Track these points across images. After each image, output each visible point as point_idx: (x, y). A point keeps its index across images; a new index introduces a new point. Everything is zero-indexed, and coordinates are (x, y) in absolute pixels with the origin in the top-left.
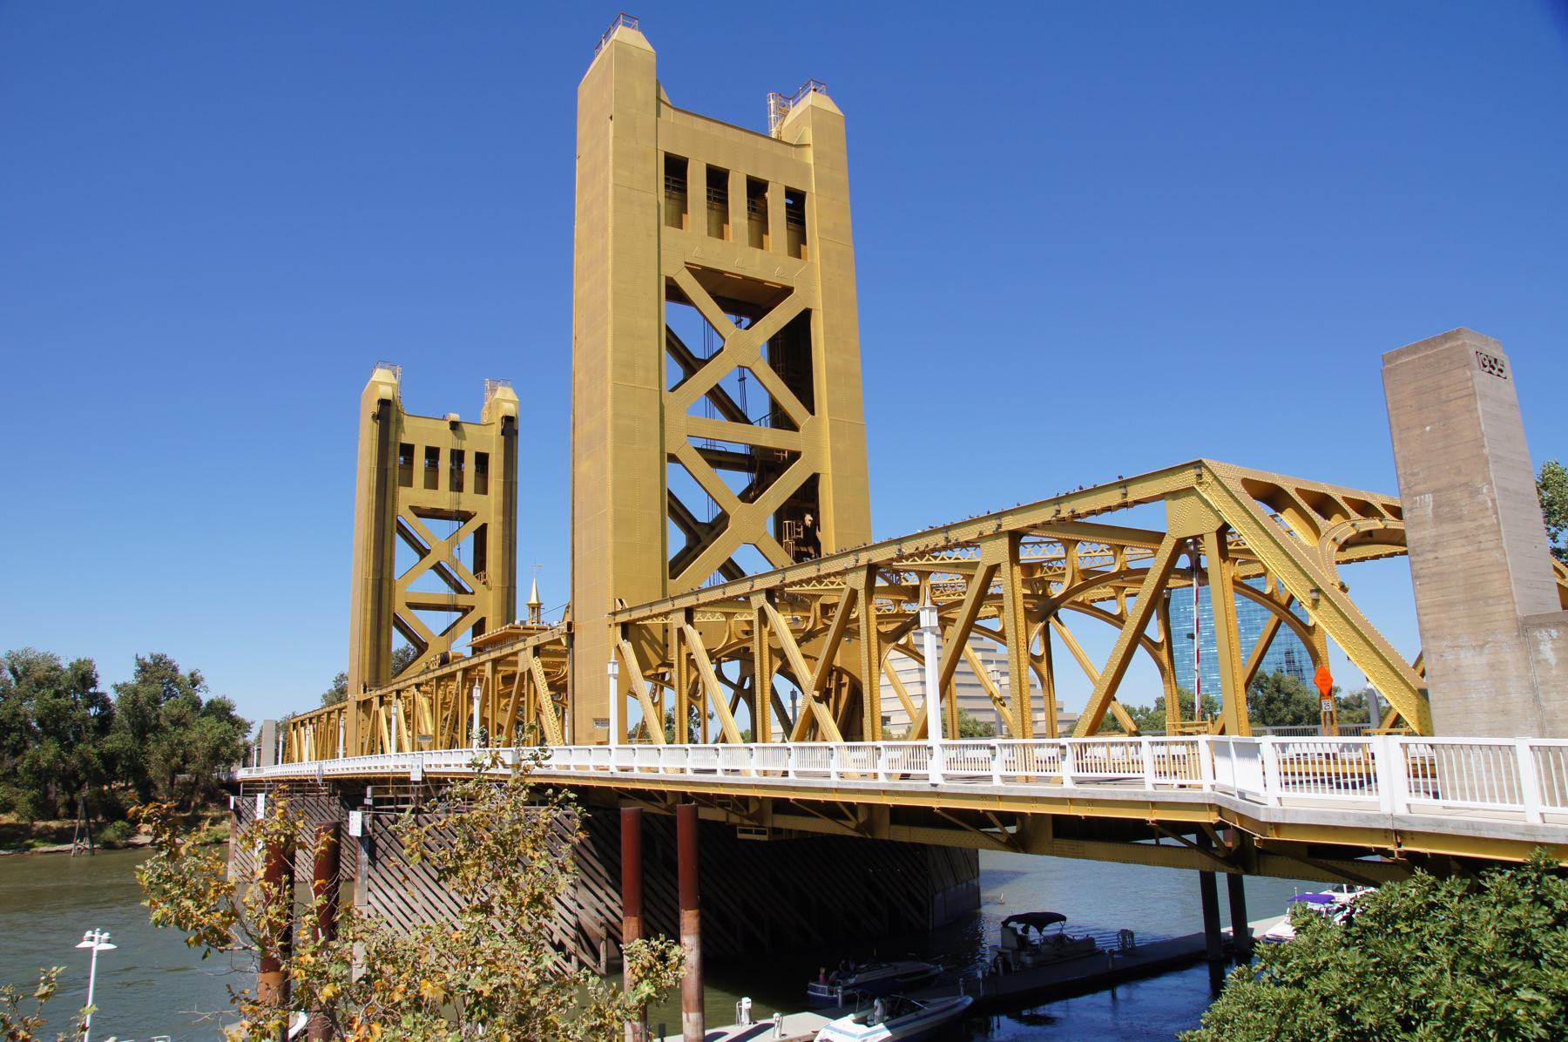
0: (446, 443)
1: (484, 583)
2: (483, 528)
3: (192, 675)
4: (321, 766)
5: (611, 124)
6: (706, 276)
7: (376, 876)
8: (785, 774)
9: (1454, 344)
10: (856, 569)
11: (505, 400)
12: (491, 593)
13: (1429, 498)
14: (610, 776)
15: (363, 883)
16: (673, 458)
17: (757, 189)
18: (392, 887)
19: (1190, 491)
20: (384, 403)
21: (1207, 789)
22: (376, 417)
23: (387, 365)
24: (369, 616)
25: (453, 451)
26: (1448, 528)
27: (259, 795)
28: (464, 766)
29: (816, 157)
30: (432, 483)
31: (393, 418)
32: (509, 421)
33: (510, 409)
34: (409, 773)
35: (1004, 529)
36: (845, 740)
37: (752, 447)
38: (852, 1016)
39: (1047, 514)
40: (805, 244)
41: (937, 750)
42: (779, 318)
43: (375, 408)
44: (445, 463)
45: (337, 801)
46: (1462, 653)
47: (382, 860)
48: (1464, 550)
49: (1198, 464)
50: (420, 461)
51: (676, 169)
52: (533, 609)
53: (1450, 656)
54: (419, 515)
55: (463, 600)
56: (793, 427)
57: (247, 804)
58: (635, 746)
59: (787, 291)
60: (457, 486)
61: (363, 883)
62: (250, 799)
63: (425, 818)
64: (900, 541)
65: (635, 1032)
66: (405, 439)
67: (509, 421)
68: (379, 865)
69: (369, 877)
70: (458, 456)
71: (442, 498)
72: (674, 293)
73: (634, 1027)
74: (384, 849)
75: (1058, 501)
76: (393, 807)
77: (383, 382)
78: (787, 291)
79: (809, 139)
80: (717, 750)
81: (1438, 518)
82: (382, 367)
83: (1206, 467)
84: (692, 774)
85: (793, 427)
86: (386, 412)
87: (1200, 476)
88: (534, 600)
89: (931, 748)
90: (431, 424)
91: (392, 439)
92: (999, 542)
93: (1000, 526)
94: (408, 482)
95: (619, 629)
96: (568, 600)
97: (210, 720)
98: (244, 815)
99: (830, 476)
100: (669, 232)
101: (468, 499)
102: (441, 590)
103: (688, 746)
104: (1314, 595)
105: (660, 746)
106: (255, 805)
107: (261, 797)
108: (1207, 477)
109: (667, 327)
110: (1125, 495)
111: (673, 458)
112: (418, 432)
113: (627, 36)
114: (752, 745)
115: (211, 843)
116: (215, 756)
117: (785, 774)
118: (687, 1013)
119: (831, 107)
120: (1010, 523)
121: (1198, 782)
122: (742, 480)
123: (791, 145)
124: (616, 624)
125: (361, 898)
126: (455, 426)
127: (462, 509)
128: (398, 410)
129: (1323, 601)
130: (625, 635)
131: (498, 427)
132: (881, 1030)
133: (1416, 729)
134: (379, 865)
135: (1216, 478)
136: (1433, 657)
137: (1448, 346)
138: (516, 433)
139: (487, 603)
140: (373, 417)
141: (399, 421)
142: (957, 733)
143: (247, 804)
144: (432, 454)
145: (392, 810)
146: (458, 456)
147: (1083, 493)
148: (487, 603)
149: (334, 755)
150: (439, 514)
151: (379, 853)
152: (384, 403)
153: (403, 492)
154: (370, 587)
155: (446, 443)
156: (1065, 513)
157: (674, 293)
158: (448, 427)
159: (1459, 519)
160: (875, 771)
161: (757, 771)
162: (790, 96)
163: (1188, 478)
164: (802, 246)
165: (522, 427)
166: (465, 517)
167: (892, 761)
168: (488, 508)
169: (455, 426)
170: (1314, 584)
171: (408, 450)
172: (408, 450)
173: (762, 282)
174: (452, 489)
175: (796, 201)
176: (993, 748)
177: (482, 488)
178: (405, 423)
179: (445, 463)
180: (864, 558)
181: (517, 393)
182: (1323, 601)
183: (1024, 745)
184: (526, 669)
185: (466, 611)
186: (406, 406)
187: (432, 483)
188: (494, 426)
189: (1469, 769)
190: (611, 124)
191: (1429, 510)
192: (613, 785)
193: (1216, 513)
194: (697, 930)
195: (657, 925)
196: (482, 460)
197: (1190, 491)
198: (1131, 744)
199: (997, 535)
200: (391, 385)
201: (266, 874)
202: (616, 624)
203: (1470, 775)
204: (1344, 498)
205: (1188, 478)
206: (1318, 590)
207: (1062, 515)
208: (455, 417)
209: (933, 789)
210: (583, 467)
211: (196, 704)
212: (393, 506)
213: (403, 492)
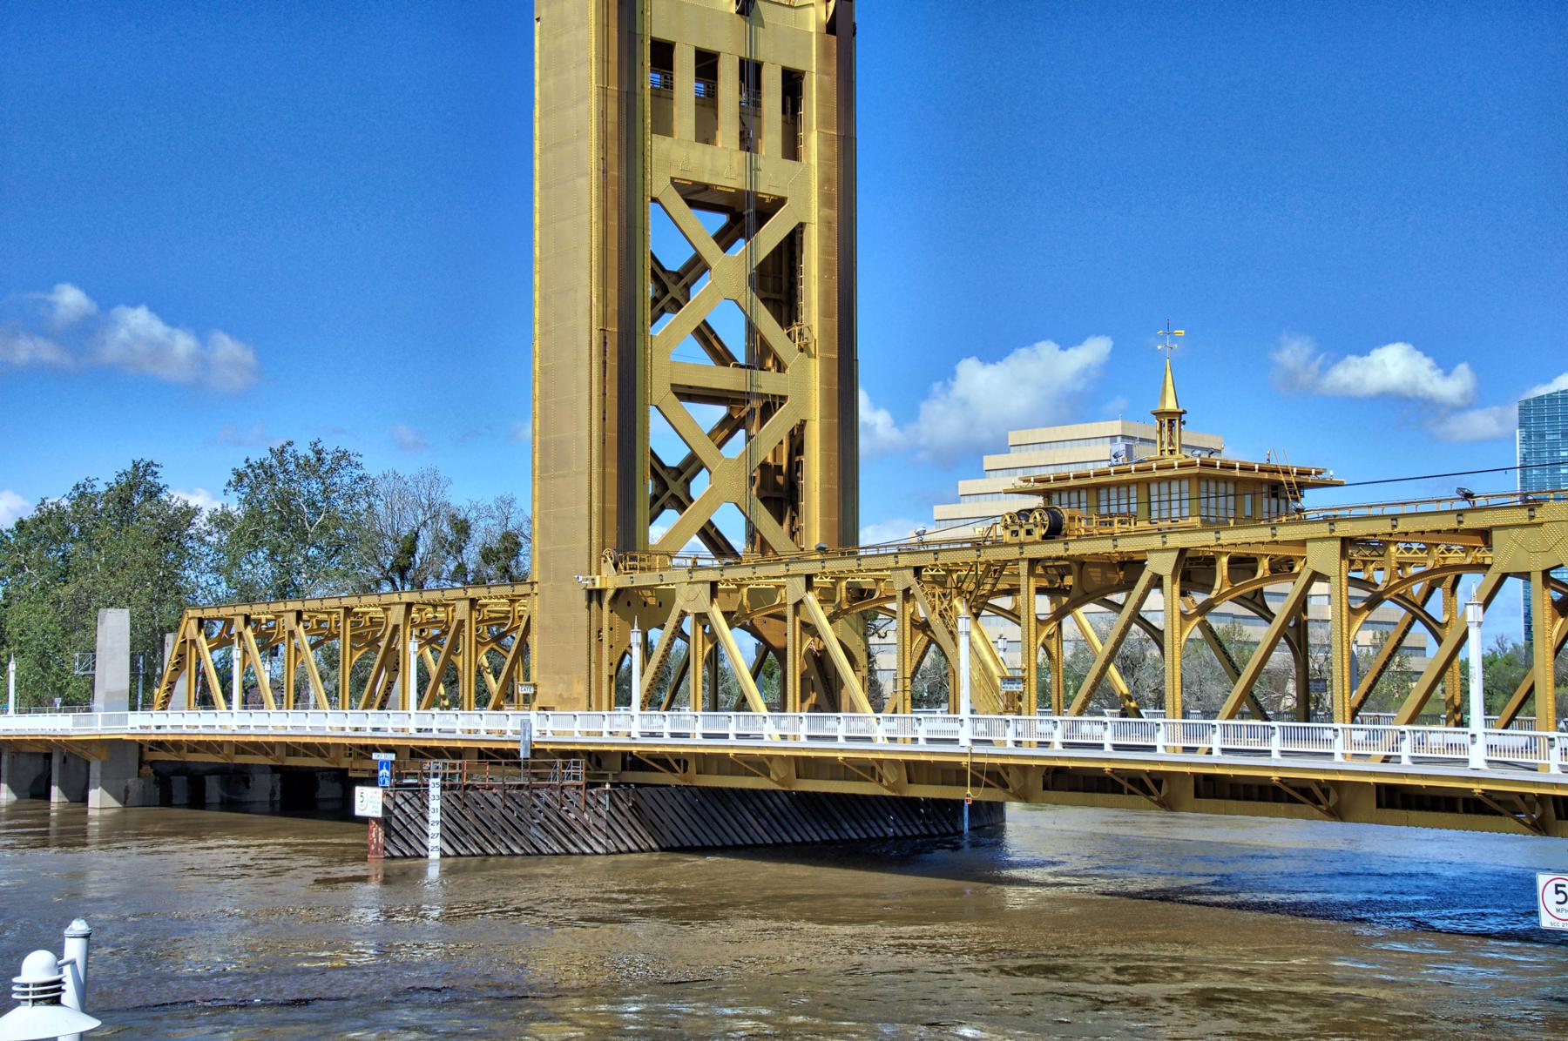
4: (526, 725)
30: (706, 134)
41: (636, 718)
42: (770, 236)
54: (692, 204)
55: (768, 382)
59: (779, 202)
60: (747, 142)
70: (750, 72)
78: (779, 202)
80: (664, 716)
84: (844, 741)
88: (1170, 405)
89: (961, 720)
94: (664, 126)
101: (773, 176)
103: (348, 711)
109: (652, 254)
121: (1547, 762)
153: (659, 146)
160: (600, 730)
161: (1165, 747)
167: (395, 722)
171: (663, 54)
176: (1106, 723)
177: (792, 149)
183: (1174, 723)
196: (792, 82)
198: (1528, 721)
201: (316, 787)
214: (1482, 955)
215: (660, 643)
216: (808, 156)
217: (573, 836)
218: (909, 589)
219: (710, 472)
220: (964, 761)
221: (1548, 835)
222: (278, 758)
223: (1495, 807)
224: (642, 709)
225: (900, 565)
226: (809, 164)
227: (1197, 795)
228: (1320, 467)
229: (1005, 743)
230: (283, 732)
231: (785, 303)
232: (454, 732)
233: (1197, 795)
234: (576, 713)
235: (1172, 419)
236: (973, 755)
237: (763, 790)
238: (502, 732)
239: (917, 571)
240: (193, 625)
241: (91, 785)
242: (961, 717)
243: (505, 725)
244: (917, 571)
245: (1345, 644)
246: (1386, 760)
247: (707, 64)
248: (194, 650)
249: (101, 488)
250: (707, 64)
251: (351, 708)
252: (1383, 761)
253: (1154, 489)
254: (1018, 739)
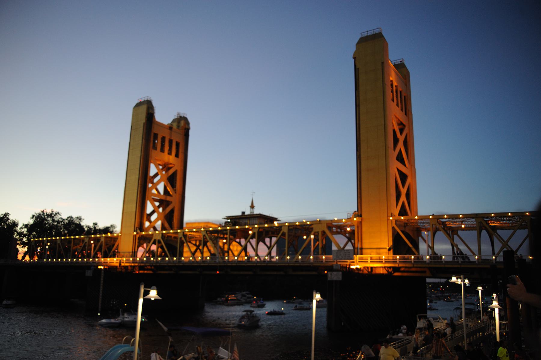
42: (171, 172)
55: (169, 198)
213: (154, 151)
247: (163, 139)
250: (163, 139)
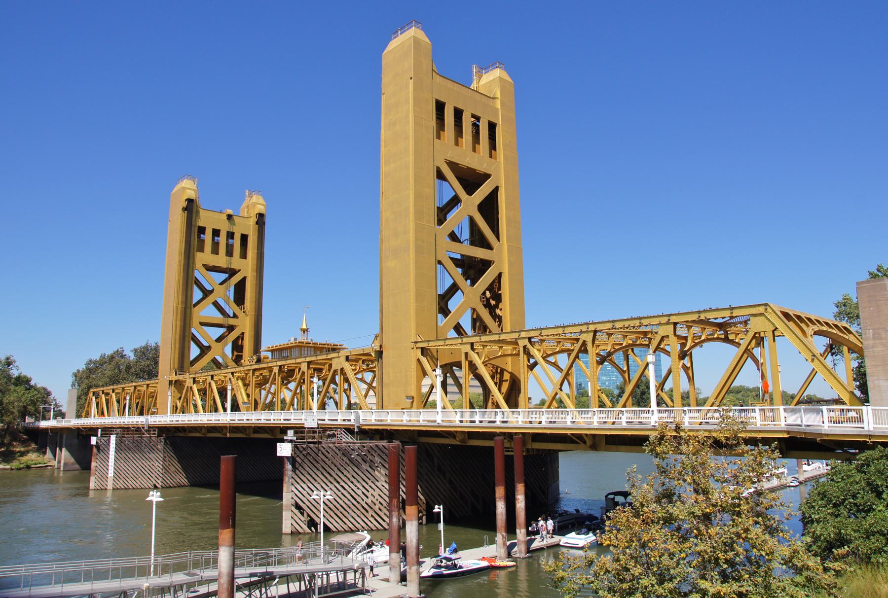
0: (224, 227)
1: (244, 312)
2: (243, 281)
3: (8, 359)
4: (147, 419)
5: (411, 82)
6: (452, 165)
7: (296, 477)
8: (540, 423)
9: (882, 282)
10: (587, 332)
11: (257, 203)
12: (248, 318)
13: (871, 331)
14: (437, 425)
15: (289, 481)
16: (440, 262)
17: (458, 113)
18: (304, 483)
19: (762, 314)
20: (190, 201)
21: (783, 425)
22: (185, 209)
23: (189, 177)
24: (178, 329)
25: (228, 232)
26: (877, 341)
27: (112, 436)
28: (282, 420)
29: (502, 104)
31: (194, 211)
32: (261, 216)
33: (261, 209)
34: (304, 424)
35: (671, 321)
36: (510, 408)
37: (462, 255)
38: (574, 533)
39: (695, 317)
40: (495, 150)
41: (440, 413)
43: (185, 204)
44: (222, 240)
45: (163, 441)
46: (880, 381)
47: (299, 469)
48: (882, 349)
49: (766, 305)
50: (208, 237)
51: (440, 107)
52: (304, 332)
53: (876, 382)
54: (208, 270)
55: (232, 322)
56: (489, 247)
57: (103, 442)
58: (421, 410)
59: (487, 176)
60: (229, 253)
61: (289, 481)
62: (105, 439)
63: (322, 446)
64: (614, 321)
65: (503, 537)
66: (201, 223)
67: (261, 216)
68: (297, 471)
69: (292, 477)
70: (231, 235)
71: (221, 260)
72: (440, 176)
73: (503, 535)
74: (300, 463)
75: (699, 312)
76: (305, 440)
77: (187, 188)
78: (487, 176)
79: (498, 95)
81: (874, 338)
82: (187, 179)
83: (770, 306)
85: (489, 247)
86: (191, 207)
87: (766, 309)
88: (304, 327)
90: (216, 215)
91: (193, 223)
92: (668, 326)
93: (669, 320)
94: (201, 249)
95: (420, 350)
96: (378, 331)
97: (21, 389)
98: (101, 448)
99: (507, 274)
100: (437, 141)
101: (236, 262)
102: (217, 316)
104: (813, 357)
105: (595, 409)
106: (109, 442)
107: (113, 438)
108: (769, 310)
110: (732, 313)
111: (440, 262)
112: (208, 219)
113: (413, 32)
114: (303, 411)
115: (23, 468)
116: (24, 413)
117: (540, 423)
118: (520, 529)
119: (507, 78)
120: (673, 319)
121: (779, 423)
122: (224, 276)
123: (490, 97)
124: (417, 348)
125: (288, 488)
126: (230, 217)
127: (232, 267)
128: (197, 206)
129: (816, 360)
130: (422, 354)
131: (254, 220)
132: (592, 536)
133: (611, 406)
134: (297, 471)
135: (773, 311)
136: (871, 382)
137: (879, 283)
138: (264, 223)
139: (245, 325)
140: (183, 209)
141: (198, 212)
142: (598, 406)
143: (103, 442)
144: (216, 233)
145: (304, 442)
146: (231, 235)
147: (711, 310)
148: (245, 325)
149: (88, 415)
150: (215, 269)
151: (297, 465)
152: (190, 201)
153: (199, 255)
154: (179, 312)
155: (224, 227)
156: (702, 317)
157: (440, 176)
158: (226, 218)
159: (881, 339)
162: (485, 68)
163: (761, 310)
164: (460, 139)
165: (267, 220)
166: (232, 272)
168: (246, 268)
169: (230, 217)
170: (812, 353)
172: (202, 230)
173: (475, 170)
174: (227, 255)
175: (492, 127)
177: (244, 255)
178: (201, 214)
179: (222, 240)
180: (592, 328)
181: (265, 199)
182: (816, 360)
184: (339, 368)
185: (231, 328)
186: (202, 203)
187: (215, 250)
188: (252, 219)
189: (882, 418)
190: (411, 82)
191: (871, 335)
192: (439, 429)
193: (773, 324)
194: (524, 493)
195: (440, 501)
196: (244, 238)
197: (762, 314)
199: (668, 323)
200: (194, 190)
202: (417, 348)
203: (882, 420)
204: (794, 315)
205: (761, 310)
206: (814, 356)
207: (701, 318)
208: (230, 212)
209: (653, 427)
210: (390, 264)
211: (9, 377)
212: (193, 263)
213: (199, 255)
214: (500, 491)
215: (69, 403)
216: (499, 159)
217: (316, 464)
218: (526, 346)
219: (463, 294)
220: (228, 425)
221: (596, 450)
222: (203, 434)
223: (447, 435)
224: (231, 411)
225: (589, 330)
226: (499, 162)
227: (607, 444)
228: (341, 343)
229: (593, 422)
230: (417, 424)
231: (239, 299)
232: (270, 420)
233: (607, 444)
234: (389, 411)
235: (305, 331)
236: (230, 424)
237: (433, 444)
238: (418, 421)
239: (530, 339)
240: (92, 393)
241: (496, 485)
242: (437, 410)
243: (387, 417)
244: (530, 339)
245: (467, 381)
246: (614, 423)
248: (191, 393)
249: (15, 376)
251: (255, 411)
252: (700, 425)
253: (303, 349)
254: (573, 420)
